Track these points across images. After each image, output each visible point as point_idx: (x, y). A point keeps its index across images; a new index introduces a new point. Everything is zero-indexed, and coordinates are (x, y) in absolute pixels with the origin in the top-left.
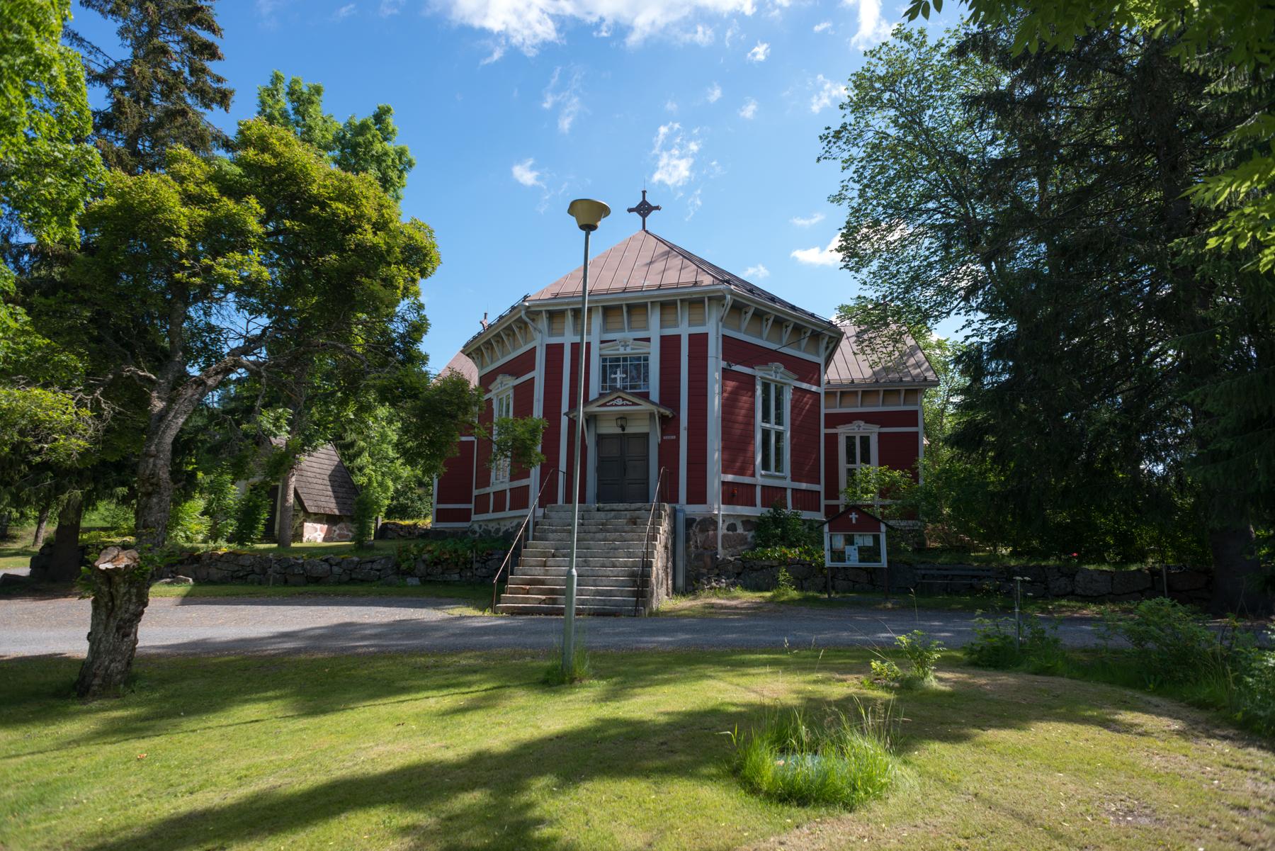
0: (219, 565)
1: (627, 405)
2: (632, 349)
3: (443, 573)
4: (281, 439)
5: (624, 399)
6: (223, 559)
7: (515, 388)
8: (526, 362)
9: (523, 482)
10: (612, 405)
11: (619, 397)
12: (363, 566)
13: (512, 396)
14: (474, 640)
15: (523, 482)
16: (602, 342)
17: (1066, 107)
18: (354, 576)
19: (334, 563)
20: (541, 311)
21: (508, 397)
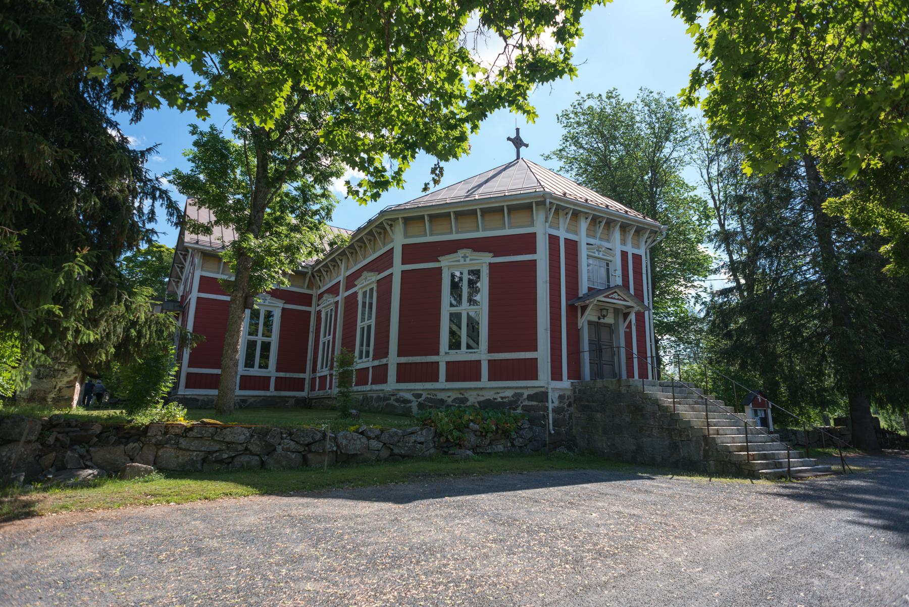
0: (183, 443)
1: (620, 300)
2: (603, 255)
3: (490, 444)
4: (716, 299)
5: (619, 295)
6: (191, 434)
7: (378, 281)
8: (385, 260)
9: (384, 361)
10: (612, 298)
11: (616, 292)
12: (407, 438)
13: (375, 289)
14: (844, 503)
15: (384, 361)
16: (588, 244)
17: (297, 159)
18: (396, 451)
19: (372, 435)
20: (398, 219)
21: (372, 290)
